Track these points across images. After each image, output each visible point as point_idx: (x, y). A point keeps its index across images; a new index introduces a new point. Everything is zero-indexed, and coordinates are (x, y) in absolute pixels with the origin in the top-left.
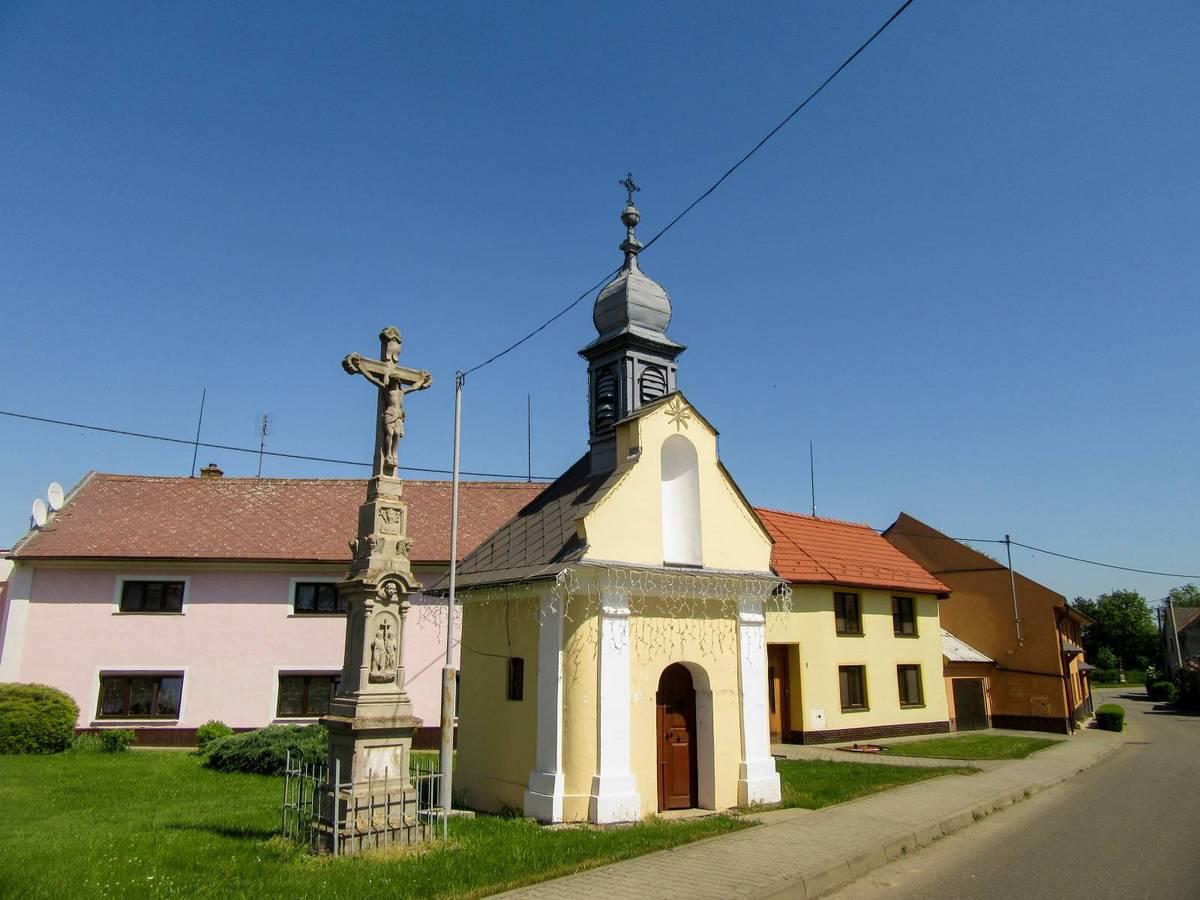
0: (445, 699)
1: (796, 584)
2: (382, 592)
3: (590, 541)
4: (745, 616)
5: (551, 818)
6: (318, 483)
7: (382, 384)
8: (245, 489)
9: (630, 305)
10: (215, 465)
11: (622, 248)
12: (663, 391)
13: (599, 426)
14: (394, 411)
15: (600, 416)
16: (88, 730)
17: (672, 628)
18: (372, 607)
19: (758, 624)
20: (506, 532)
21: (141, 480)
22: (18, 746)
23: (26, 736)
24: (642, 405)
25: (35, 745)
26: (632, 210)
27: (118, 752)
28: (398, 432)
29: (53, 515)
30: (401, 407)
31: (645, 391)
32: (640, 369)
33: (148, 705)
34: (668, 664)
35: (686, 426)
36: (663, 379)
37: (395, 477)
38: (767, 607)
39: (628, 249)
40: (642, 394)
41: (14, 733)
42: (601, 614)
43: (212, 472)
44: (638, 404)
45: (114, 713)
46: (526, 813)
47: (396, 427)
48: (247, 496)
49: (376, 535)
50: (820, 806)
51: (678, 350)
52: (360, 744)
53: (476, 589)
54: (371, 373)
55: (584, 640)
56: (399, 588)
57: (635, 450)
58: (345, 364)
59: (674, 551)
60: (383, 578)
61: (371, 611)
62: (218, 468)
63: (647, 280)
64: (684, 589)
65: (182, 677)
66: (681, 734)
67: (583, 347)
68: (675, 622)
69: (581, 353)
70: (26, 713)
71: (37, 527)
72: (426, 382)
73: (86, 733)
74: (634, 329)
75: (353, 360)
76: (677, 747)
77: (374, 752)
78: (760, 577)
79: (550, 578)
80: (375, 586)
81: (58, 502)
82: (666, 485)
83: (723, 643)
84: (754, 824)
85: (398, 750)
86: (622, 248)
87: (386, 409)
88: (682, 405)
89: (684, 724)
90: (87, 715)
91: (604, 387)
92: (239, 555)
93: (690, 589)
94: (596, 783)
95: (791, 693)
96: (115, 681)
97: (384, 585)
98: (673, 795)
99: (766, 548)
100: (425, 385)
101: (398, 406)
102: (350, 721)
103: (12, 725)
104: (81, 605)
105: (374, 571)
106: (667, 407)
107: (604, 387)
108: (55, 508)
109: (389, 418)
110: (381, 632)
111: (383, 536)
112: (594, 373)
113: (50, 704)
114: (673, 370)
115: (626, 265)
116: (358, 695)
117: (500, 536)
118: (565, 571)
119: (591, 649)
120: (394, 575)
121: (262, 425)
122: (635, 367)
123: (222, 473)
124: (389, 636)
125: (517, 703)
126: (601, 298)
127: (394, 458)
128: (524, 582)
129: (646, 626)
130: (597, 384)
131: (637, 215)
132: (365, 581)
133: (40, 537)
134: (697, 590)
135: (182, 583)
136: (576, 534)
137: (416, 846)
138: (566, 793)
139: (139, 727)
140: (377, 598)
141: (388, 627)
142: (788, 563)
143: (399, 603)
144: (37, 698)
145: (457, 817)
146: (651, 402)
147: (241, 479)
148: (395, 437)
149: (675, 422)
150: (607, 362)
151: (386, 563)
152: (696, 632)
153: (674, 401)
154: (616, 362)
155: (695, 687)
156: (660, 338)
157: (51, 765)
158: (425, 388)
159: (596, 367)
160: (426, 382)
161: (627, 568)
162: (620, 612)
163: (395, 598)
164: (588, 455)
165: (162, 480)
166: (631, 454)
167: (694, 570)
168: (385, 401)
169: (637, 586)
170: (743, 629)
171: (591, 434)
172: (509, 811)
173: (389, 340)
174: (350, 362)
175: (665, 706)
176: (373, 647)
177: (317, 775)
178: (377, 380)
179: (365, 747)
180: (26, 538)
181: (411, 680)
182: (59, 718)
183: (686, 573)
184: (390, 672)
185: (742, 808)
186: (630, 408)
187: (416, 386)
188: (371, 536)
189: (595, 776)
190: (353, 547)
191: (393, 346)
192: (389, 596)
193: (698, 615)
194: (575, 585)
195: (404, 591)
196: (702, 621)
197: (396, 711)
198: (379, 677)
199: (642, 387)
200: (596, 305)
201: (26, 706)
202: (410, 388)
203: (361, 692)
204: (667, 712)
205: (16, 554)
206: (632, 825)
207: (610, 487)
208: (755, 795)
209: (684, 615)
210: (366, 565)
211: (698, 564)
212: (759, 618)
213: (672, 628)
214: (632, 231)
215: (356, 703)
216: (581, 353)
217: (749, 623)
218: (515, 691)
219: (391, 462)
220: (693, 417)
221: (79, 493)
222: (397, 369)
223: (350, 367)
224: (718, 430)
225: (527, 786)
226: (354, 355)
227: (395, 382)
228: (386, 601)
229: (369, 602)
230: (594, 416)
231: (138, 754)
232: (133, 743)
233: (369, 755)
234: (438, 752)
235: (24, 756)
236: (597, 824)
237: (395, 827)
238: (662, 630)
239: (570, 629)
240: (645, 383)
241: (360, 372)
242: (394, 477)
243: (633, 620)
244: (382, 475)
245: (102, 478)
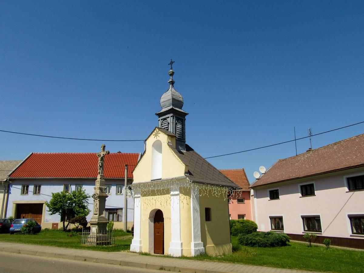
152: (148, 198)
196: (161, 196)
245: (280, 161)
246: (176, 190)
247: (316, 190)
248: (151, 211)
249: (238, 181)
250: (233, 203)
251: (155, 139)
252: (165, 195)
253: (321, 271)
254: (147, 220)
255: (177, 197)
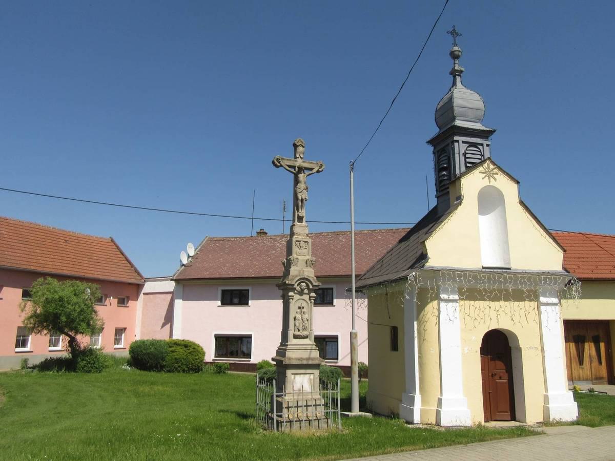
0: (353, 350)
1: (585, 281)
2: (298, 288)
3: (429, 255)
4: (543, 299)
5: (413, 420)
6: (313, 235)
7: (295, 172)
8: (276, 241)
9: (455, 108)
10: (263, 230)
11: (451, 73)
12: (481, 159)
13: (440, 186)
14: (301, 186)
15: (440, 179)
16: (211, 363)
17: (490, 307)
18: (293, 296)
19: (555, 304)
20: (390, 254)
21: (228, 239)
22: (179, 369)
23: (182, 364)
24: (466, 169)
25: (186, 369)
26: (456, 48)
27: (222, 374)
28: (304, 198)
29: (190, 258)
30: (305, 183)
31: (468, 160)
32: (463, 147)
33: (237, 351)
34: (488, 330)
35: (495, 179)
36: (481, 152)
37: (304, 223)
38: (563, 295)
39: (455, 73)
40: (466, 163)
41: (177, 363)
42: (439, 300)
43: (262, 233)
44: (463, 169)
45: (222, 355)
46: (401, 417)
47: (302, 195)
48: (277, 244)
49: (294, 256)
50: (600, 424)
51: (491, 132)
52: (289, 372)
53: (370, 287)
54: (287, 165)
55: (429, 315)
56: (307, 285)
57: (459, 198)
58: (273, 162)
59: (490, 258)
60: (298, 280)
61: (293, 299)
62: (264, 231)
63: (469, 91)
64: (494, 283)
65: (251, 337)
66: (502, 374)
67: (429, 139)
68: (492, 304)
69: (428, 142)
70: (182, 354)
71: (183, 265)
72: (320, 168)
73: (209, 364)
74: (458, 123)
75: (278, 160)
76: (500, 382)
77: (297, 377)
78: (554, 274)
79: (405, 279)
80: (293, 285)
81: (192, 253)
82: (481, 217)
83: (529, 316)
84: (540, 433)
85: (312, 376)
86: (451, 73)
87: (297, 185)
88: (492, 167)
89: (504, 368)
90: (210, 355)
91: (442, 161)
92: (273, 275)
93: (500, 283)
94: (440, 401)
95: (613, 352)
96: (222, 339)
97: (299, 284)
98: (498, 412)
99: (560, 255)
100: (320, 170)
101: (303, 183)
102: (283, 359)
103: (176, 359)
104: (205, 301)
105: (293, 276)
106: (481, 169)
107: (442, 161)
108: (191, 255)
109: (298, 190)
110: (299, 310)
111: (298, 257)
112: (436, 153)
113: (191, 350)
114: (488, 145)
115: (454, 84)
116: (288, 345)
117: (388, 256)
118: (414, 273)
119: (434, 320)
120: (304, 279)
121: (283, 206)
122: (460, 146)
123: (266, 233)
124: (304, 313)
125: (395, 353)
126: (439, 107)
127: (303, 213)
128: (392, 281)
129: (471, 306)
130: (439, 160)
131: (459, 51)
132: (287, 282)
133: (184, 270)
134: (505, 283)
135: (248, 290)
136: (422, 253)
137: (322, 430)
138: (422, 406)
139: (234, 362)
140: (296, 292)
141: (303, 308)
142: (606, 268)
143: (309, 294)
144: (186, 346)
145: (360, 416)
146: (471, 167)
147: (274, 236)
148: (302, 200)
149: (487, 178)
150: (443, 146)
151: (300, 272)
152: (507, 310)
153: (486, 165)
154: (448, 145)
155: (510, 345)
156: (478, 126)
157: (190, 379)
158: (321, 171)
159: (437, 149)
160: (320, 168)
161: (454, 271)
162: (451, 297)
163: (306, 291)
164: (436, 208)
165: (238, 239)
166: (457, 200)
167: (504, 270)
168: (297, 181)
169: (461, 281)
170: (543, 308)
171: (437, 191)
172: (394, 415)
173: (298, 146)
174: (275, 161)
175: (489, 357)
176: (295, 319)
177: (262, 384)
178: (292, 170)
179: (293, 374)
180: (179, 270)
181: (361, 343)
182: (196, 356)
183: (497, 273)
184: (305, 333)
185: (546, 423)
186: (457, 173)
187: (314, 171)
188: (291, 257)
189: (440, 397)
190: (284, 264)
191: (300, 149)
192: (302, 290)
193: (507, 299)
194: (420, 281)
195: (311, 287)
197: (310, 354)
198: (299, 335)
199: (466, 158)
200: (436, 112)
201: (180, 350)
202: (311, 172)
203: (289, 343)
204: (491, 360)
205: (175, 278)
206: (463, 428)
207: (442, 222)
208: (554, 416)
209: (496, 299)
210: (289, 273)
211: (508, 266)
212: (555, 300)
213: (490, 307)
214: (457, 62)
215: (286, 350)
216: (428, 142)
217: (547, 304)
218: (395, 346)
219: (300, 215)
220: (500, 173)
221: (202, 247)
222: (303, 162)
223: (276, 164)
224: (518, 180)
225: (401, 401)
226: (277, 157)
227: (301, 170)
228: (301, 293)
229: (291, 294)
230: (438, 179)
231: (231, 375)
232: (230, 369)
233: (295, 378)
234: (350, 379)
235: (181, 373)
236: (441, 426)
237: (310, 419)
238: (483, 309)
239: (421, 307)
240: (468, 156)
241: (281, 166)
242: (303, 223)
243: (462, 302)
244: (296, 223)
245: (211, 240)
246: (453, 292)
247: (337, 298)
248: (516, 333)
249: (85, 265)
250: (111, 305)
251: (486, 182)
252: (522, 303)
253: (514, 428)
254: (477, 352)
255: (554, 309)
